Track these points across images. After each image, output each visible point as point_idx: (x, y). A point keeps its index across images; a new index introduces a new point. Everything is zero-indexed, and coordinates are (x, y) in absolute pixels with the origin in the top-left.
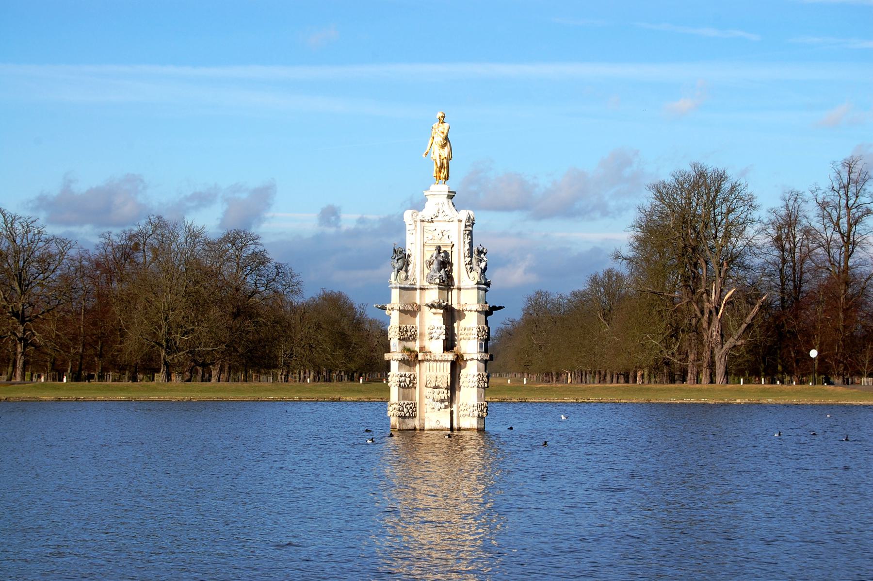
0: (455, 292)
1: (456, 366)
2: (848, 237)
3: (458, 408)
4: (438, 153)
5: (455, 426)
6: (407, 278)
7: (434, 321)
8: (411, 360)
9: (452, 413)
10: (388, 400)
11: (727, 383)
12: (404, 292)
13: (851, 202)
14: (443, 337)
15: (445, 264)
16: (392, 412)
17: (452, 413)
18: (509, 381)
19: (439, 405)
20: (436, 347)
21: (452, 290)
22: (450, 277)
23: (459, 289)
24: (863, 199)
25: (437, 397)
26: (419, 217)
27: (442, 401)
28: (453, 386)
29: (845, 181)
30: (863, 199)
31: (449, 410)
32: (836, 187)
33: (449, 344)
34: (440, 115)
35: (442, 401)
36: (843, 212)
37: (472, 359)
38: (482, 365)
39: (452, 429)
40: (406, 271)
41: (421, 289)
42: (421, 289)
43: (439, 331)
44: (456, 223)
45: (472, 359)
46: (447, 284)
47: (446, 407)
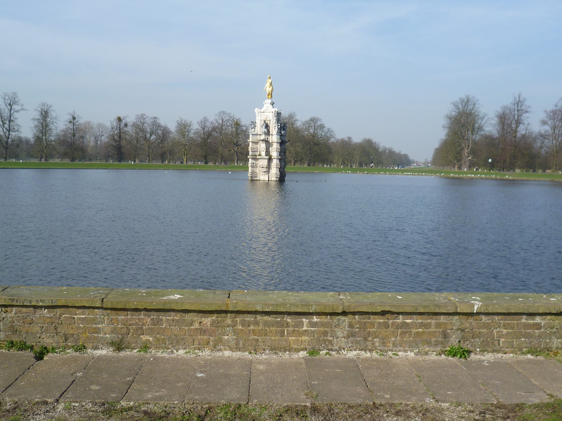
0: (271, 136)
1: (270, 160)
2: (517, 120)
3: (271, 174)
4: (269, 89)
5: (270, 180)
6: (254, 131)
7: (263, 146)
8: (255, 158)
9: (269, 176)
10: (248, 171)
11: (469, 170)
12: (253, 136)
13: (519, 109)
14: (265, 151)
15: (267, 126)
16: (249, 175)
17: (269, 176)
18: (465, 169)
19: (264, 173)
20: (263, 154)
21: (270, 135)
22: (269, 131)
23: (272, 135)
24: (523, 108)
25: (263, 171)
26: (260, 111)
27: (265, 172)
28: (269, 167)
29: (517, 101)
30: (523, 108)
31: (268, 175)
32: (513, 103)
33: (268, 153)
34: (269, 76)
35: (265, 172)
36: (516, 112)
37: (274, 158)
38: (278, 161)
39: (269, 180)
40: (255, 129)
41: (260, 135)
42: (260, 135)
43: (264, 149)
44: (271, 113)
45: (274, 158)
46: (268, 133)
47: (266, 174)
